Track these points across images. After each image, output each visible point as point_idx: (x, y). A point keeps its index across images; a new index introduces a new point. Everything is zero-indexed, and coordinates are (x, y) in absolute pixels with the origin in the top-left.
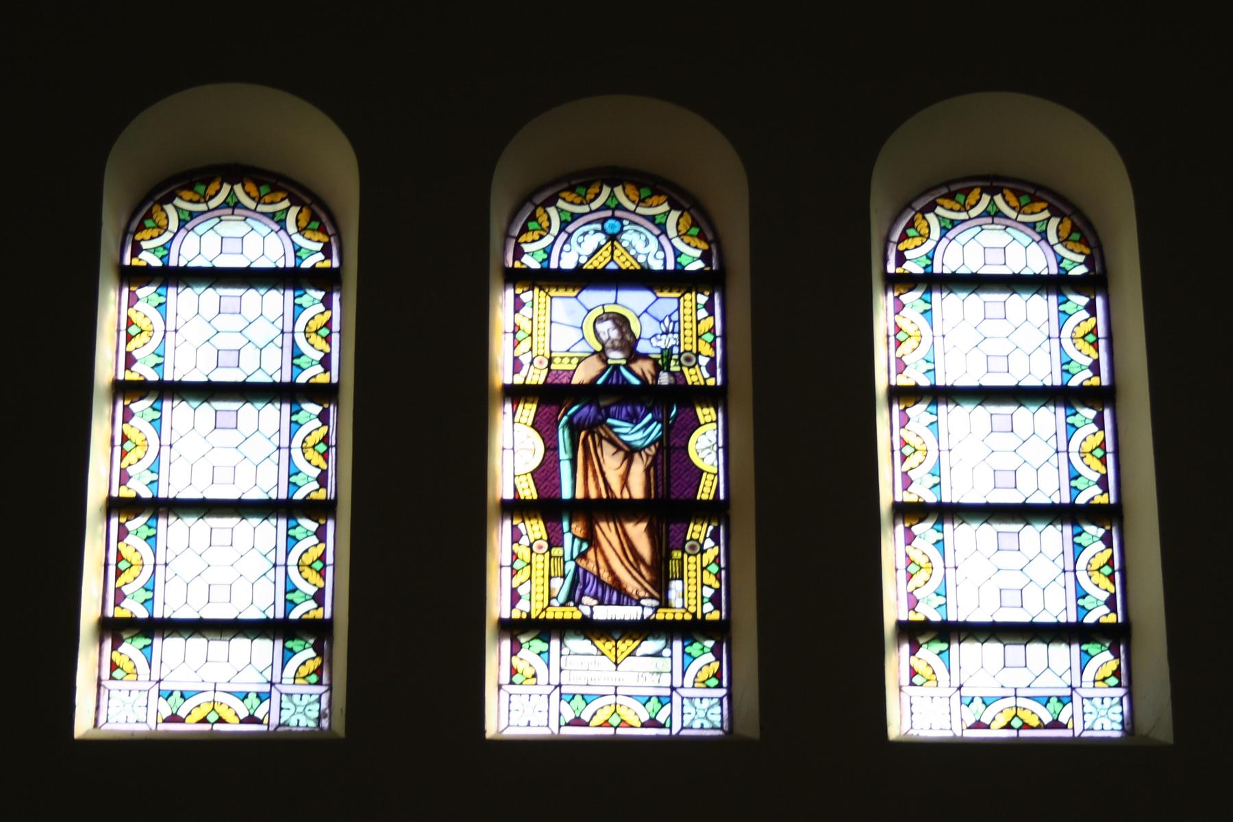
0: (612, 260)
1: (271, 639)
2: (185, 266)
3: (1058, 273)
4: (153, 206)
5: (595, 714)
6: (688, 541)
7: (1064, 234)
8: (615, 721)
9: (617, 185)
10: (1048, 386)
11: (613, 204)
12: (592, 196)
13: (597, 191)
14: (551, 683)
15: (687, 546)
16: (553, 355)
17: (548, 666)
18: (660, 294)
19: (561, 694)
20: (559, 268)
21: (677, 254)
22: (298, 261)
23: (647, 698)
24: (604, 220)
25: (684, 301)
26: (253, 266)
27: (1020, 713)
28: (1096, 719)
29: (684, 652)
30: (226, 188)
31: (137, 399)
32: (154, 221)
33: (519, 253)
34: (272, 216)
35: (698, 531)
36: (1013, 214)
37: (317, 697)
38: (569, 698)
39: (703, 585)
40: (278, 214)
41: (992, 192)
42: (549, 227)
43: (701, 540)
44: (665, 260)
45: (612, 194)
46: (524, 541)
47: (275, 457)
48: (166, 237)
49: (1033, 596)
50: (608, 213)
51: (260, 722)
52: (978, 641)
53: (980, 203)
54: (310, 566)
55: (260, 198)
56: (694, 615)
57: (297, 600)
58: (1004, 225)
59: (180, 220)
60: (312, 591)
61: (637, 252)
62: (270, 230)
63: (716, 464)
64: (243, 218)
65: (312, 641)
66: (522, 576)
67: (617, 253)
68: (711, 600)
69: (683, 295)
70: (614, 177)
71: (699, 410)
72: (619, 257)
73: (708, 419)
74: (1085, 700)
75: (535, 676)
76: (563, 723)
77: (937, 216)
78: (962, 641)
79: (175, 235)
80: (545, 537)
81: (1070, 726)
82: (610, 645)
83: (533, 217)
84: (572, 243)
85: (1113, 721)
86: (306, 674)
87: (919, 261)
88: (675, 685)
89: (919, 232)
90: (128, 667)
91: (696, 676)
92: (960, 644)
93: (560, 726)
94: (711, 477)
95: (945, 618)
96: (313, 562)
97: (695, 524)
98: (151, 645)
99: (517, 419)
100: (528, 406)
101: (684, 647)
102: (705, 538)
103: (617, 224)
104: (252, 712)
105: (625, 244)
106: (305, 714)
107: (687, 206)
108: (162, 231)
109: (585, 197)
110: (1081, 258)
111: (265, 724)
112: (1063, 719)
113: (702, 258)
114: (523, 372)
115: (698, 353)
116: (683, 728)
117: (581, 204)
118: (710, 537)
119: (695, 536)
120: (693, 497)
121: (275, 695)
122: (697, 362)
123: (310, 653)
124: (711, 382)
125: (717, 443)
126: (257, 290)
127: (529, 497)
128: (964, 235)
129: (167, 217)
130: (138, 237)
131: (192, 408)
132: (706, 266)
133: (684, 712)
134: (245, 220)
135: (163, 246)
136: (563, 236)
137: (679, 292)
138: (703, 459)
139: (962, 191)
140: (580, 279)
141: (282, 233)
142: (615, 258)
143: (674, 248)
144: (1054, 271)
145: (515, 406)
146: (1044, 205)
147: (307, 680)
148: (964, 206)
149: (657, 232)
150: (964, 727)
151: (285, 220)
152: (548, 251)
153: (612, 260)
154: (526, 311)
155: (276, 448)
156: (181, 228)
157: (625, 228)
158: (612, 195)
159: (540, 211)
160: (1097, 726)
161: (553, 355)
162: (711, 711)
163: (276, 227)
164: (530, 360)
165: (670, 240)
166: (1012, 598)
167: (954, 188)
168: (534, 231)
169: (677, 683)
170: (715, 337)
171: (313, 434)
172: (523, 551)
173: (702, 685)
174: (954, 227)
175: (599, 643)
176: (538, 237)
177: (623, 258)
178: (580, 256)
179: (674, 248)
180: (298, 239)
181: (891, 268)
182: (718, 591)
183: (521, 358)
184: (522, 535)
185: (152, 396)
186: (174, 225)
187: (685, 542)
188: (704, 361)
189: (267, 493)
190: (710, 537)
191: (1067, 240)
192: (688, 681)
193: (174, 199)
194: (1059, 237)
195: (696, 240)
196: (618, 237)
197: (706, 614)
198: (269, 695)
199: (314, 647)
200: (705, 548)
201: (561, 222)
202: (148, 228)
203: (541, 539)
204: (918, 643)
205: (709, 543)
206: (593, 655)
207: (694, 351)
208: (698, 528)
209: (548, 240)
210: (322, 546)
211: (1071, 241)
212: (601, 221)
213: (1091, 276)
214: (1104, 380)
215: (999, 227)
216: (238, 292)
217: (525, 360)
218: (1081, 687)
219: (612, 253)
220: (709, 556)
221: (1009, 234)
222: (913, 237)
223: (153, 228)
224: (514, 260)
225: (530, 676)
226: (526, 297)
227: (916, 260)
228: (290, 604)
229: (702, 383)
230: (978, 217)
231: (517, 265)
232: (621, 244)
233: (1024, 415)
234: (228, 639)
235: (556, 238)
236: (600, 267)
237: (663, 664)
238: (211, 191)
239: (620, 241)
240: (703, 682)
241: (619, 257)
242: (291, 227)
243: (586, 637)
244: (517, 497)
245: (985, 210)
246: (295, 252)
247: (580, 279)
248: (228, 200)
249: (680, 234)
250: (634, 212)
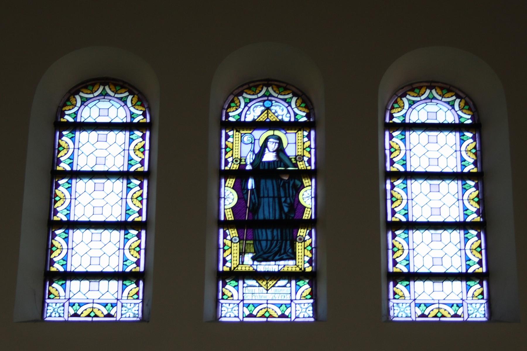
0: (268, 118)
1: (116, 280)
2: (83, 122)
3: (459, 123)
4: (397, 98)
5: (258, 312)
6: (298, 236)
7: (134, 103)
8: (267, 315)
9: (269, 86)
10: (455, 172)
11: (268, 94)
12: (258, 92)
13: (260, 89)
14: (239, 299)
15: (298, 239)
16: (242, 158)
17: (238, 291)
18: (288, 132)
19: (244, 304)
20: (245, 121)
21: (296, 114)
22: (132, 119)
23: (248, 305)
24: (264, 101)
25: (298, 134)
26: (113, 121)
27: (441, 310)
28: (399, 312)
29: (296, 285)
30: (101, 88)
31: (397, 180)
32: (398, 105)
33: (392, 117)
34: (121, 99)
35: (302, 232)
36: (440, 98)
37: (409, 304)
38: (247, 305)
39: (304, 256)
40: (288, 100)
41: (268, 86)
42: (240, 105)
43: (304, 236)
44: (290, 117)
45: (267, 90)
46: (229, 237)
47: (120, 202)
48: (76, 109)
49: (105, 260)
50: (266, 98)
51: (112, 316)
52: (451, 281)
53: (99, 90)
54: (134, 249)
55: (116, 91)
56: (301, 269)
57: (471, 264)
58: (436, 103)
59: (82, 101)
60: (477, 260)
61: (278, 115)
62: (120, 106)
63: (311, 204)
64: (436, 104)
65: (307, 281)
66: (228, 252)
67: (270, 115)
68: (308, 262)
69: (298, 132)
70: (268, 83)
71: (304, 180)
72: (271, 117)
73: (308, 184)
74: (468, 305)
75: (232, 296)
76: (417, 316)
77: (407, 99)
78: (72, 280)
79: (80, 108)
80: (237, 235)
81: (462, 316)
82: (265, 283)
83: (233, 101)
84: (251, 111)
85: (481, 314)
86: (305, 295)
87: (399, 118)
88: (292, 299)
89: (400, 106)
90: (401, 294)
91: (301, 295)
92: (414, 282)
93: (68, 317)
94: (309, 210)
95: (65, 270)
96: (135, 248)
97: (301, 229)
98: (65, 283)
99: (226, 185)
100: (231, 180)
101: (296, 282)
102: (306, 235)
103: (270, 103)
104: (251, 312)
105: (273, 111)
106: (404, 312)
107: (136, 92)
108: (402, 109)
109: (255, 92)
110: (469, 117)
111: (115, 317)
112: (112, 313)
113: (306, 116)
114: (229, 166)
115: (304, 156)
116: (296, 318)
117: (253, 95)
118: (308, 235)
119: (301, 234)
120: (301, 217)
121: (465, 304)
122: (303, 159)
123: (307, 286)
124: (309, 168)
125: (311, 195)
126: (96, 132)
127: (230, 219)
128: (419, 107)
129: (403, 103)
130: (393, 111)
131: (447, 183)
132: (308, 120)
133: (237, 311)
134: (109, 101)
135: (74, 113)
136: (247, 108)
137: (295, 130)
138: (305, 202)
139: (417, 88)
140: (255, 125)
141: (453, 110)
142: (269, 117)
143: (294, 112)
144: (457, 122)
145: (226, 180)
146: (453, 94)
147: (133, 298)
148: (419, 94)
149: (287, 105)
150: (69, 316)
151: (126, 101)
152: (240, 115)
153: (268, 118)
154: (230, 139)
155: (77, 199)
156: (82, 105)
157: (273, 104)
158: (267, 90)
159: (399, 99)
160: (400, 315)
161: (242, 158)
162: (406, 309)
163: (123, 104)
164: (232, 160)
165: (292, 109)
166: (436, 212)
167: (251, 85)
168: (233, 107)
169: (293, 298)
170: (58, 149)
171: (136, 193)
172: (228, 242)
173: (304, 298)
174: (87, 100)
175: (260, 282)
176: (235, 109)
177: (272, 117)
178: (254, 116)
179: (294, 112)
180: (132, 109)
181: (387, 120)
182: (311, 258)
183: (228, 159)
184: (228, 235)
185: (402, 179)
186: (79, 104)
187: (297, 237)
188: (306, 159)
189: (116, 218)
190: (308, 235)
191: (463, 109)
192: (298, 297)
193: (79, 93)
194: (460, 108)
195: (304, 109)
196: (270, 108)
197: (306, 268)
198: (116, 304)
199: (308, 283)
200: (305, 239)
201: (245, 103)
202: (68, 105)
203: (236, 236)
204: (397, 282)
205: (307, 237)
206: (256, 287)
207: (302, 155)
208: (302, 230)
209: (239, 111)
210: (479, 241)
211: (464, 109)
212: (263, 101)
213: (268, 121)
214: (142, 269)
215: (107, 100)
216: (106, 132)
217: (230, 160)
218: (467, 299)
219: (268, 116)
220: (308, 242)
221: (438, 106)
222: (397, 108)
223: (70, 105)
224: (390, 120)
225: (230, 296)
226: (231, 133)
227: (234, 117)
228: (468, 266)
229: (305, 168)
230: (425, 99)
231: (391, 122)
232: (271, 111)
233: (446, 234)
234: (442, 281)
235: (243, 109)
236: (264, 120)
237: (287, 290)
238: (422, 92)
239: (271, 110)
240: (304, 297)
241: (271, 117)
242: (129, 104)
243: (254, 279)
244: (225, 219)
245: (428, 97)
246: (131, 115)
247: (255, 125)
248: (102, 93)
249: (297, 106)
250: (277, 98)
